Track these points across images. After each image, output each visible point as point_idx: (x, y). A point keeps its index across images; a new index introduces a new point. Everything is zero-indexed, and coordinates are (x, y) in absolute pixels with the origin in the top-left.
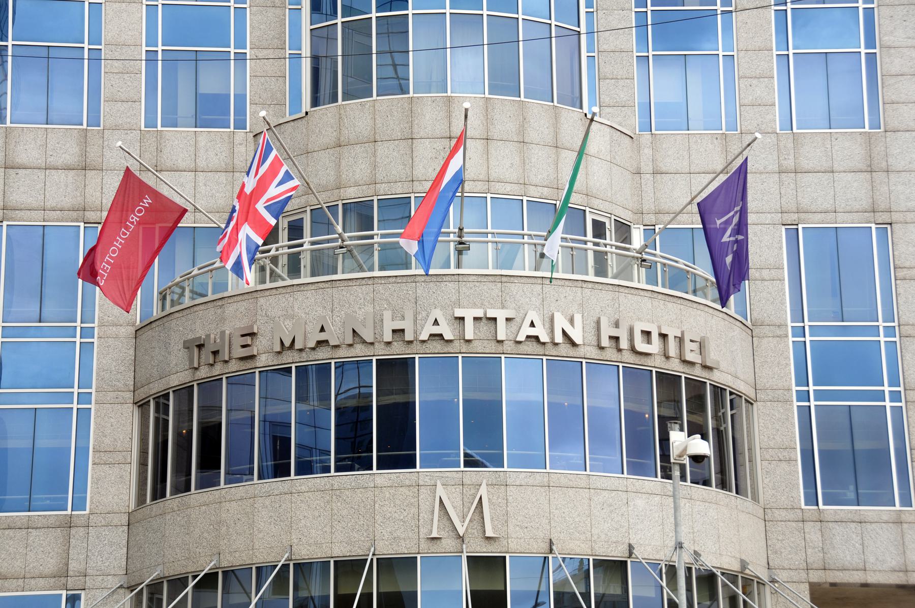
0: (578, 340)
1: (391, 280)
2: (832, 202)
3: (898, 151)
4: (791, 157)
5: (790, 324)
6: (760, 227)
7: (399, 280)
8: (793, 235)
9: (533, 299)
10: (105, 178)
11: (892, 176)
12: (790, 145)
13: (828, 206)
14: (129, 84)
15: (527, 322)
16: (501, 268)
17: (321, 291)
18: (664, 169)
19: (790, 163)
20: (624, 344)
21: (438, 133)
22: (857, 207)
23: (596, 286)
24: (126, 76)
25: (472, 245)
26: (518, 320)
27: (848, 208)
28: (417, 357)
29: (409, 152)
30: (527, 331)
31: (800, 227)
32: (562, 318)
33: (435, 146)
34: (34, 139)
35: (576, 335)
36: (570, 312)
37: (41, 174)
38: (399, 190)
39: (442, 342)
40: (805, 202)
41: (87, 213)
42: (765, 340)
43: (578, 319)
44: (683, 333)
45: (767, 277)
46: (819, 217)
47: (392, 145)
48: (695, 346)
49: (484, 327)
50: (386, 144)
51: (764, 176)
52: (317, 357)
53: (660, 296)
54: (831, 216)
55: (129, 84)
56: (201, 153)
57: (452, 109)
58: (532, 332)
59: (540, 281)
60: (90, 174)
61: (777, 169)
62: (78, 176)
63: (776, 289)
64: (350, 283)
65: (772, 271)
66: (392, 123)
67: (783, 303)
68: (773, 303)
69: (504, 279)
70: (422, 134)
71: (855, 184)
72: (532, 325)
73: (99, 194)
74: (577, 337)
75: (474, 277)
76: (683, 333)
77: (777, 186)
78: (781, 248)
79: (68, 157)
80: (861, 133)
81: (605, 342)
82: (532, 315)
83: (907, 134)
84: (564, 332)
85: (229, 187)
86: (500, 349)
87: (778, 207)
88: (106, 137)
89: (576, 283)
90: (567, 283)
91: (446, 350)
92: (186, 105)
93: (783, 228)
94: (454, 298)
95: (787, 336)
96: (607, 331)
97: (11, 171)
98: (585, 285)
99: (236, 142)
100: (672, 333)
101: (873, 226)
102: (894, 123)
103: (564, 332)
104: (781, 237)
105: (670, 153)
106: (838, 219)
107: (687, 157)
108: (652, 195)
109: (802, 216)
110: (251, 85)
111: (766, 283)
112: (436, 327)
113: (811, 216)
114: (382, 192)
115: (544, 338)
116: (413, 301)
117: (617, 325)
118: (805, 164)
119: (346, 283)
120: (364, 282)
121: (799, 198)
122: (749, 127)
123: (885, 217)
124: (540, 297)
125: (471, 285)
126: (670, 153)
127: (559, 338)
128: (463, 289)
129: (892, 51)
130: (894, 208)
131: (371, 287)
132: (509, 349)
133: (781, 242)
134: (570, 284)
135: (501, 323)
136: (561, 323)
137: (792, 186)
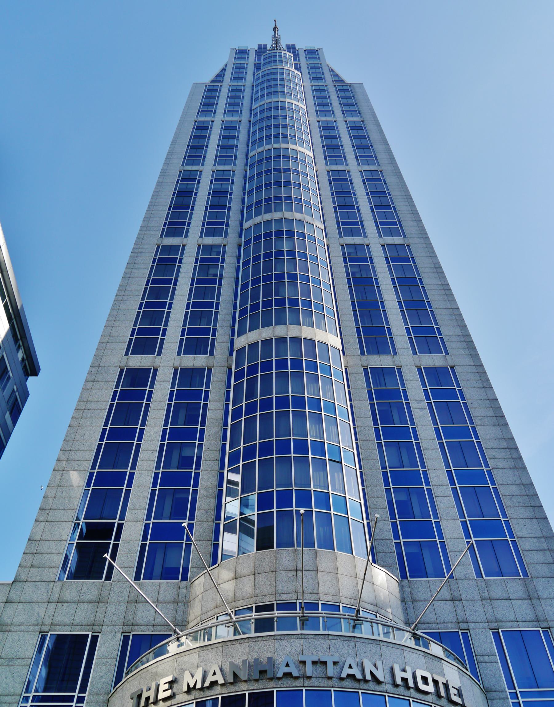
0: (381, 679)
1: (260, 639)
2: (514, 616)
3: (541, 588)
4: (486, 591)
5: (508, 691)
6: (477, 631)
7: (264, 639)
8: (496, 635)
9: (350, 651)
10: (108, 607)
11: (542, 601)
12: (484, 585)
13: (512, 618)
14: (130, 559)
15: (347, 665)
16: (328, 630)
17: (215, 650)
18: (418, 599)
19: (486, 595)
20: (411, 684)
21: (290, 568)
22: (528, 619)
23: (389, 645)
24: (129, 555)
25: (309, 619)
26: (341, 664)
27: (524, 619)
28: (275, 690)
29: (273, 578)
30: (346, 671)
31: (500, 630)
32: (370, 663)
33: (288, 575)
34: (76, 588)
35: (380, 675)
36: (374, 661)
37: (75, 606)
38: (268, 600)
39: (292, 679)
40: (499, 616)
41: (95, 627)
42: (495, 701)
43: (379, 664)
44: (447, 681)
45: (487, 661)
46: (509, 624)
47: (264, 575)
48: (456, 692)
49: (319, 669)
50: (260, 575)
51: (473, 602)
52: (210, 694)
53: (429, 656)
54: (516, 623)
55: (130, 559)
56: (162, 594)
57: (297, 555)
58: (351, 671)
59: (353, 639)
60: (100, 605)
61: (480, 598)
62: (94, 606)
63: (494, 668)
64: (234, 643)
65: (490, 657)
66: (264, 564)
67: (501, 677)
68: (494, 677)
69: (330, 637)
70: (281, 568)
71: (524, 606)
72: (350, 667)
73: (103, 616)
74: (381, 677)
75: (311, 636)
76: (447, 681)
77: (482, 608)
78: (492, 643)
79: (90, 596)
80: (519, 579)
81: (399, 682)
82: (350, 660)
83: (543, 579)
84: (372, 673)
85: (174, 611)
86: (330, 683)
87: (485, 619)
88: (113, 585)
89: (376, 642)
90: (370, 641)
91: (294, 685)
92: (158, 570)
93: (491, 631)
94: (299, 650)
95: (508, 698)
96: (399, 675)
97: (60, 605)
98: (382, 643)
99: (181, 587)
100: (441, 680)
101: (541, 630)
102: (535, 574)
103: (372, 673)
104: (490, 636)
105: (420, 590)
106: (520, 626)
107: (429, 592)
108: (413, 613)
109: (500, 624)
110: (192, 558)
111: (488, 664)
112: (287, 668)
113: (504, 624)
114: (258, 601)
115: (359, 676)
116: (273, 652)
117: (404, 670)
118: (494, 595)
119: (231, 643)
120: (242, 641)
121: (496, 614)
122: (460, 576)
123: (545, 624)
124: (354, 649)
125: (310, 641)
126: (420, 590)
127: (368, 677)
128: (305, 644)
129: (523, 539)
130: (548, 619)
131: (246, 644)
132: (336, 684)
133: (491, 639)
134: (372, 642)
135: (330, 665)
136: (368, 667)
137: (490, 607)
